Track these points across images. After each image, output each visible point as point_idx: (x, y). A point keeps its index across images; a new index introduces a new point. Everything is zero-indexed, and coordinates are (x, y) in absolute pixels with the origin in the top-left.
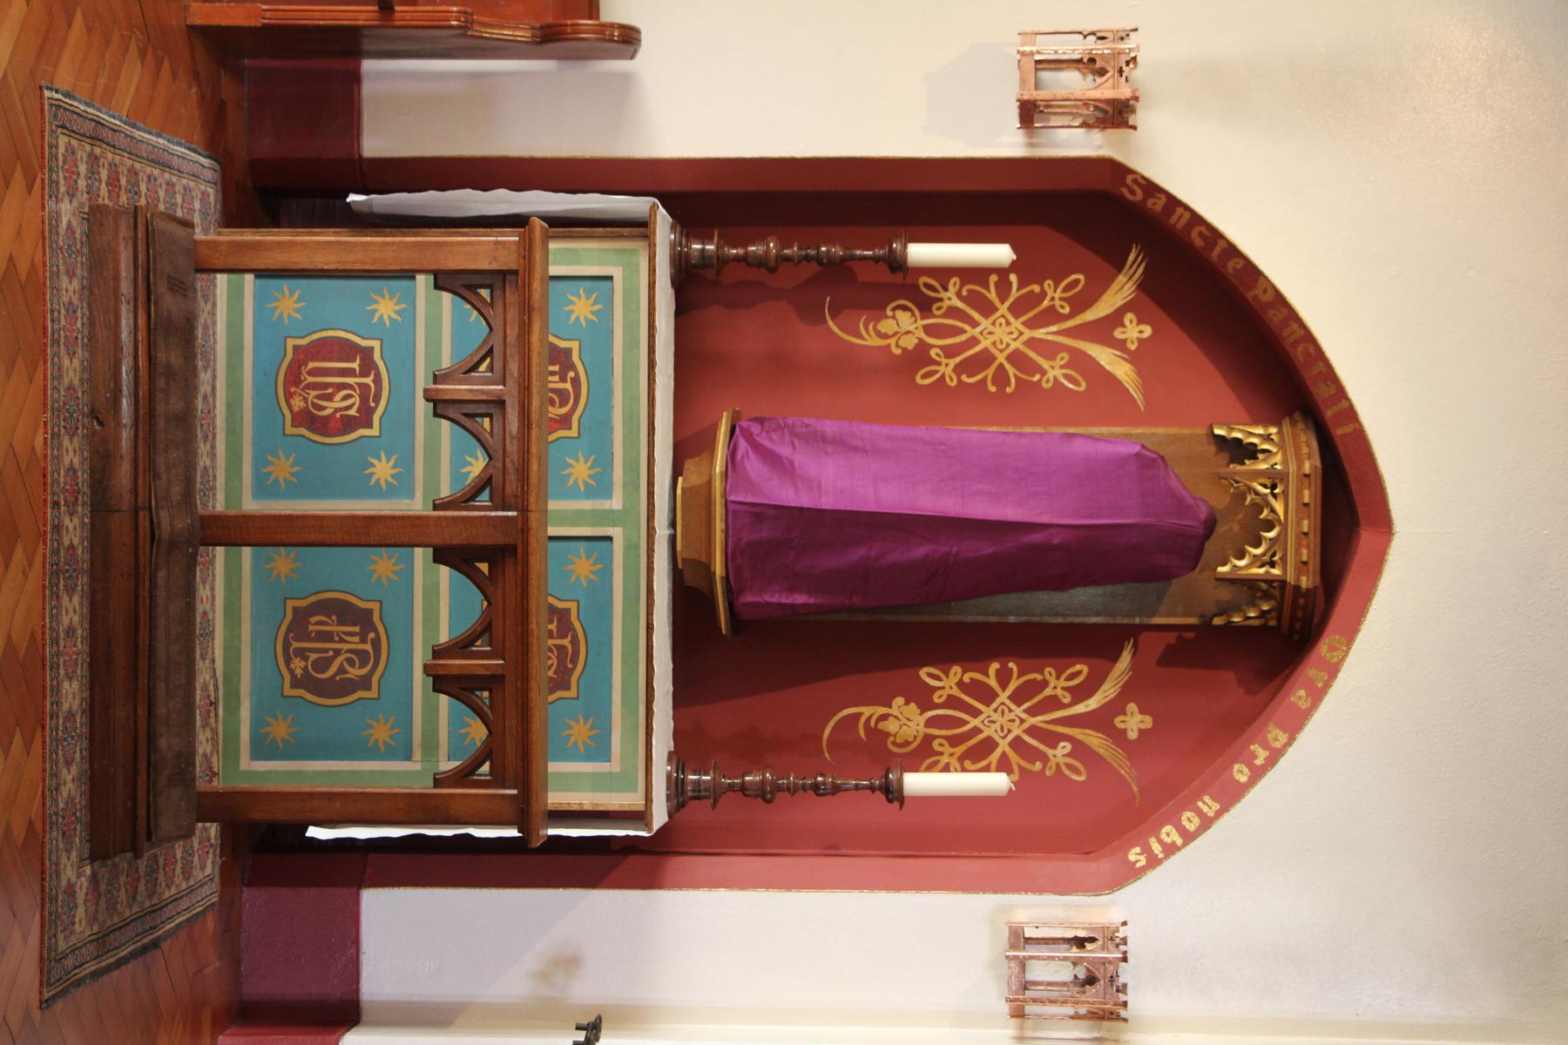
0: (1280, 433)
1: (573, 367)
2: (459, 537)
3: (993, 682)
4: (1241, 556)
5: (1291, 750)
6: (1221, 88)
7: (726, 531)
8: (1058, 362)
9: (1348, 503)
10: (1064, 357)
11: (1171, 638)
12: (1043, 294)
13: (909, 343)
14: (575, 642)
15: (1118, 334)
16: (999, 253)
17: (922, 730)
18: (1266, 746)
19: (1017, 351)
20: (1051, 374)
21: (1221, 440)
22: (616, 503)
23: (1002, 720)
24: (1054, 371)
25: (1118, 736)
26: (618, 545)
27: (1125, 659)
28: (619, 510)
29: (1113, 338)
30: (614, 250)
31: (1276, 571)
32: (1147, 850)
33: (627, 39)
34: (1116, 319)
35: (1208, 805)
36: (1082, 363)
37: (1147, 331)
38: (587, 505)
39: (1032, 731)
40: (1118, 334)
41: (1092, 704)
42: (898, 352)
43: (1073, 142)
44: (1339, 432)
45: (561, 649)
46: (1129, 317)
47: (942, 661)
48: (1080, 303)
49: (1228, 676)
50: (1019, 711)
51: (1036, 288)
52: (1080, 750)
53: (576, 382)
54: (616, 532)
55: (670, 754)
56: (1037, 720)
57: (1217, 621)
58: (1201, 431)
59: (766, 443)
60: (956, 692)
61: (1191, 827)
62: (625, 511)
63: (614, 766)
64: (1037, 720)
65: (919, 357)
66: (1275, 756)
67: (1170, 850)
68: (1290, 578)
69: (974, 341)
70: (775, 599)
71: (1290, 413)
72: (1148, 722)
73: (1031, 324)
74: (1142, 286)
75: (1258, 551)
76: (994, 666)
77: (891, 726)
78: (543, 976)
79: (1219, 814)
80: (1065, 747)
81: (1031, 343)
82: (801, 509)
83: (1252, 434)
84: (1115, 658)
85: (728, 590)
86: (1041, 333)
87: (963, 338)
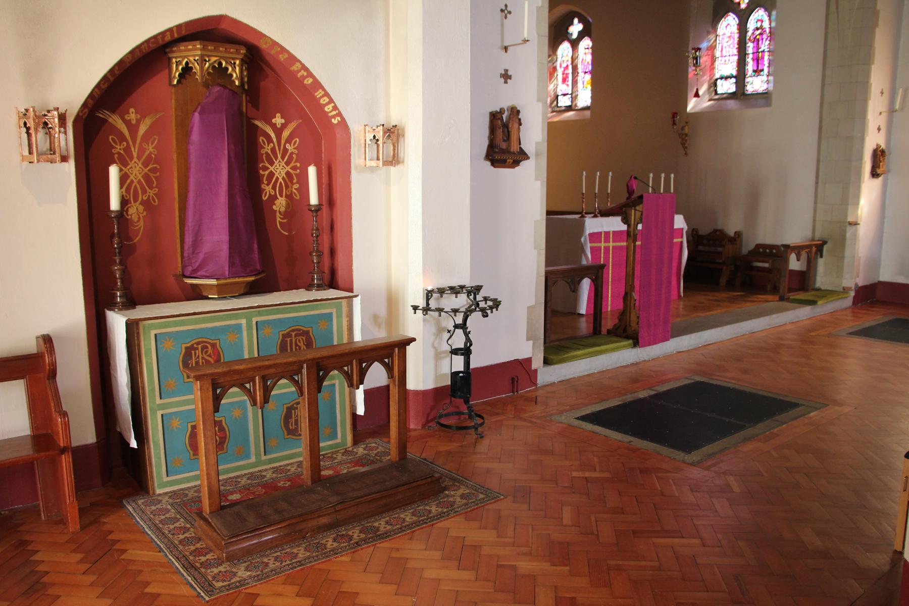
0: (176, 58)
1: (192, 345)
2: (314, 384)
3: (267, 172)
4: (231, 75)
5: (303, 62)
6: (37, 71)
7: (239, 277)
8: (146, 147)
9: (210, 32)
10: (144, 145)
11: (250, 105)
12: (118, 153)
13: (141, 208)
14: (293, 331)
15: (134, 122)
16: (114, 172)
17: (284, 198)
18: (299, 71)
19: (143, 164)
20: (152, 150)
21: (178, 81)
22: (244, 322)
23: (279, 169)
24: (150, 149)
25: (284, 126)
26: (259, 319)
27: (258, 123)
28: (244, 322)
29: (133, 123)
30: (663, 382)
31: (238, 62)
32: (334, 117)
33: (47, 340)
34: (128, 123)
35: (319, 94)
36: (146, 137)
37: (132, 110)
38: (245, 333)
39: (283, 158)
40: (134, 122)
41: (273, 135)
42: (145, 213)
43: (66, 140)
44: (184, 33)
45: (296, 335)
46: (127, 117)
47: (260, 191)
48: (122, 138)
49: (262, 84)
50: (276, 163)
51: (116, 156)
52: (289, 140)
53: (198, 344)
54: (254, 320)
55: (307, 290)
56: (279, 156)
57: (246, 87)
58: (173, 90)
59: (197, 264)
60: (270, 186)
61: (327, 100)
62: (246, 318)
63: (334, 311)
64: (279, 156)
65: (147, 204)
66: (304, 68)
67: (335, 108)
68: (241, 57)
69: (139, 182)
70: (257, 256)
71: (166, 53)
72: (278, 115)
73: (131, 158)
74: (113, 111)
75: (230, 69)
76: (261, 172)
77: (283, 209)
78: (379, 326)
79: (324, 89)
80: (288, 146)
81: (139, 158)
82: (230, 248)
83: (176, 71)
84: (257, 127)
85: (259, 273)
86: (135, 154)
87: (138, 186)
